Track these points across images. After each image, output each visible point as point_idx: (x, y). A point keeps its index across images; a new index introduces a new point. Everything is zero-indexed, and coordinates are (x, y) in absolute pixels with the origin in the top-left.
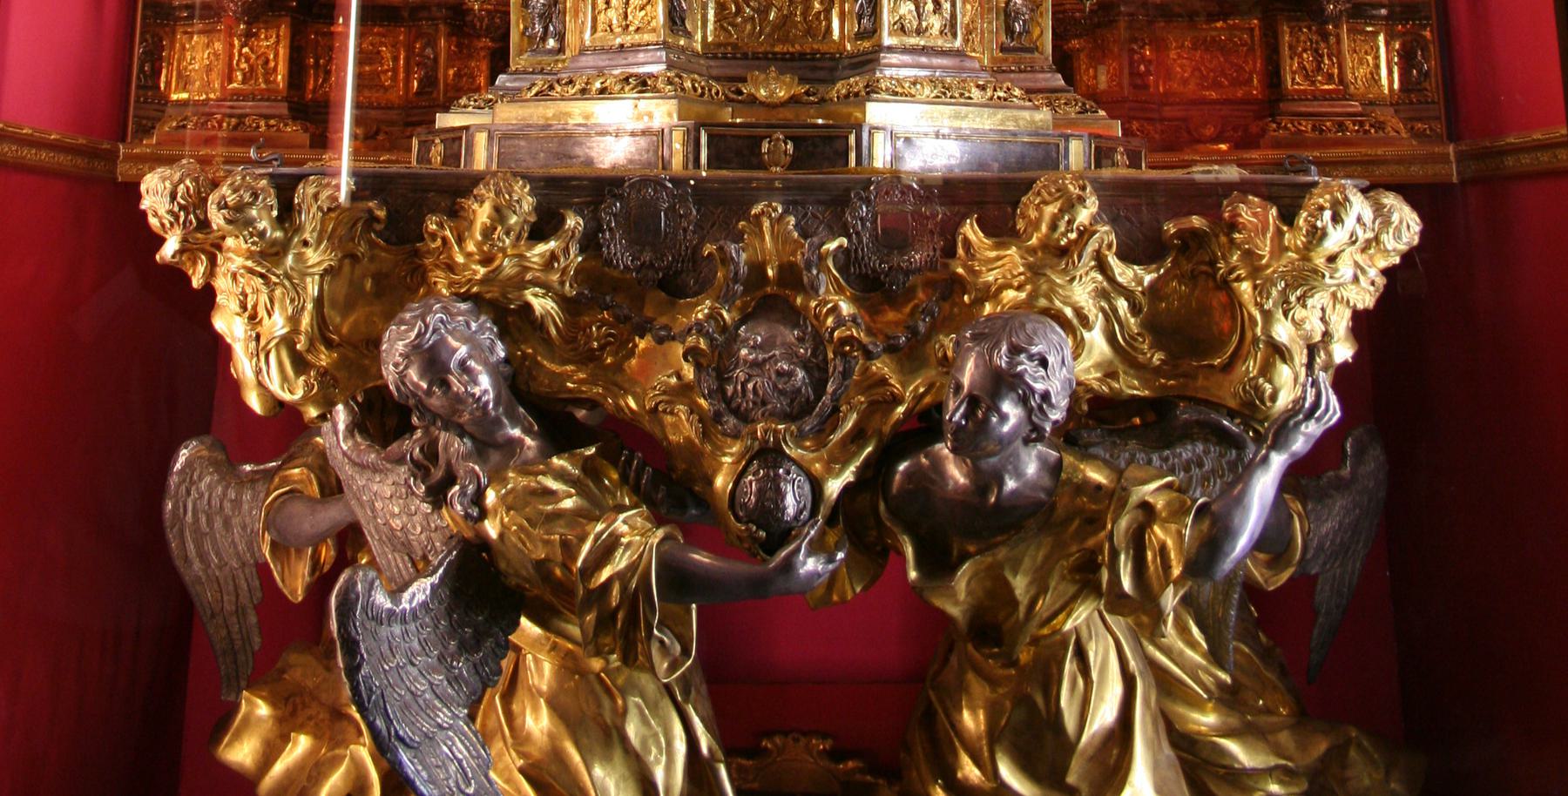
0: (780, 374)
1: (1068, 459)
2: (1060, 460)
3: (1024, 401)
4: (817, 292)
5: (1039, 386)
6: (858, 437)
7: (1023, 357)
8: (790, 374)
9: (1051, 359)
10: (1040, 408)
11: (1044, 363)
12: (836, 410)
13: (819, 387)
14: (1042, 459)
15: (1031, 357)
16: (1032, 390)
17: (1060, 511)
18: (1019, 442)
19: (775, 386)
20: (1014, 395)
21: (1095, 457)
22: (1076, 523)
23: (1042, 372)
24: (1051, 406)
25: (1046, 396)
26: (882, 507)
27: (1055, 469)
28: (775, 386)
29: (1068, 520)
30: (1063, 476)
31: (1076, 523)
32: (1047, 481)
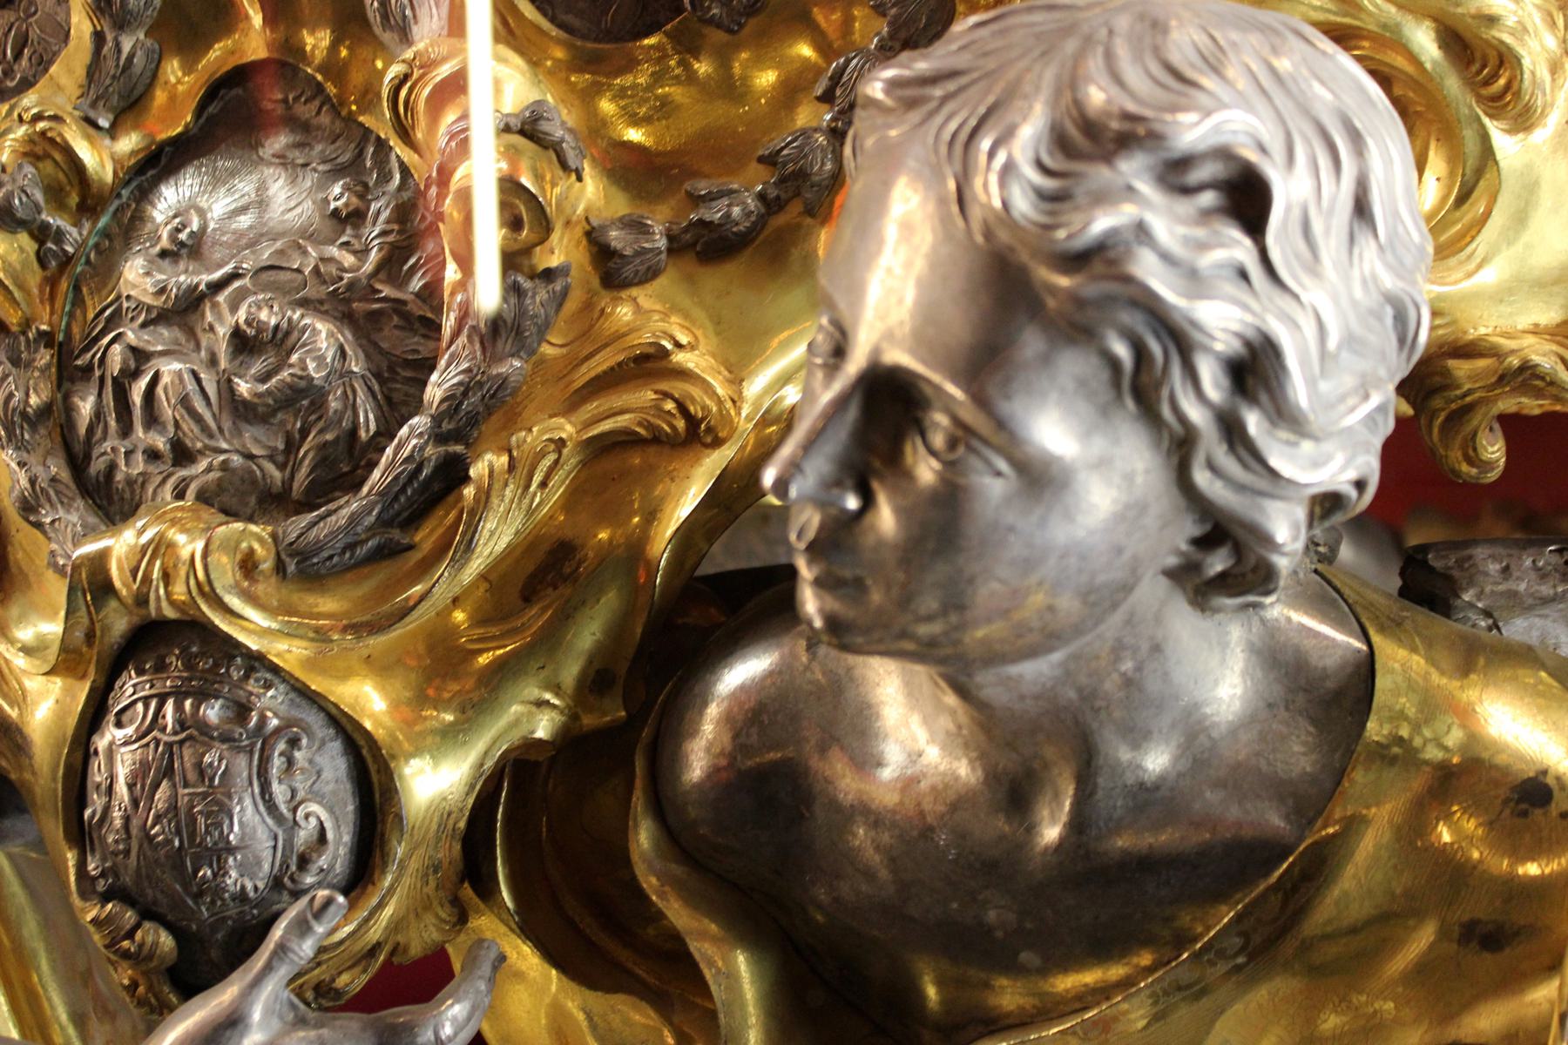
0: (243, 344)
1: (1402, 664)
2: (1366, 669)
3: (1141, 390)
4: (405, 37)
5: (1220, 320)
6: (545, 574)
7: (1133, 169)
8: (282, 341)
9: (1288, 191)
10: (1232, 430)
11: (1246, 199)
12: (453, 473)
13: (398, 384)
14: (1283, 665)
15: (1175, 174)
16: (1180, 340)
17: (1361, 875)
18: (1153, 591)
19: (227, 387)
20: (1075, 364)
21: (1524, 656)
22: (1422, 940)
23: (1240, 248)
24: (1284, 415)
25: (1255, 369)
26: (644, 837)
27: (1337, 703)
28: (227, 387)
29: (1388, 922)
30: (1375, 729)
31: (1422, 940)
32: (1298, 755)
